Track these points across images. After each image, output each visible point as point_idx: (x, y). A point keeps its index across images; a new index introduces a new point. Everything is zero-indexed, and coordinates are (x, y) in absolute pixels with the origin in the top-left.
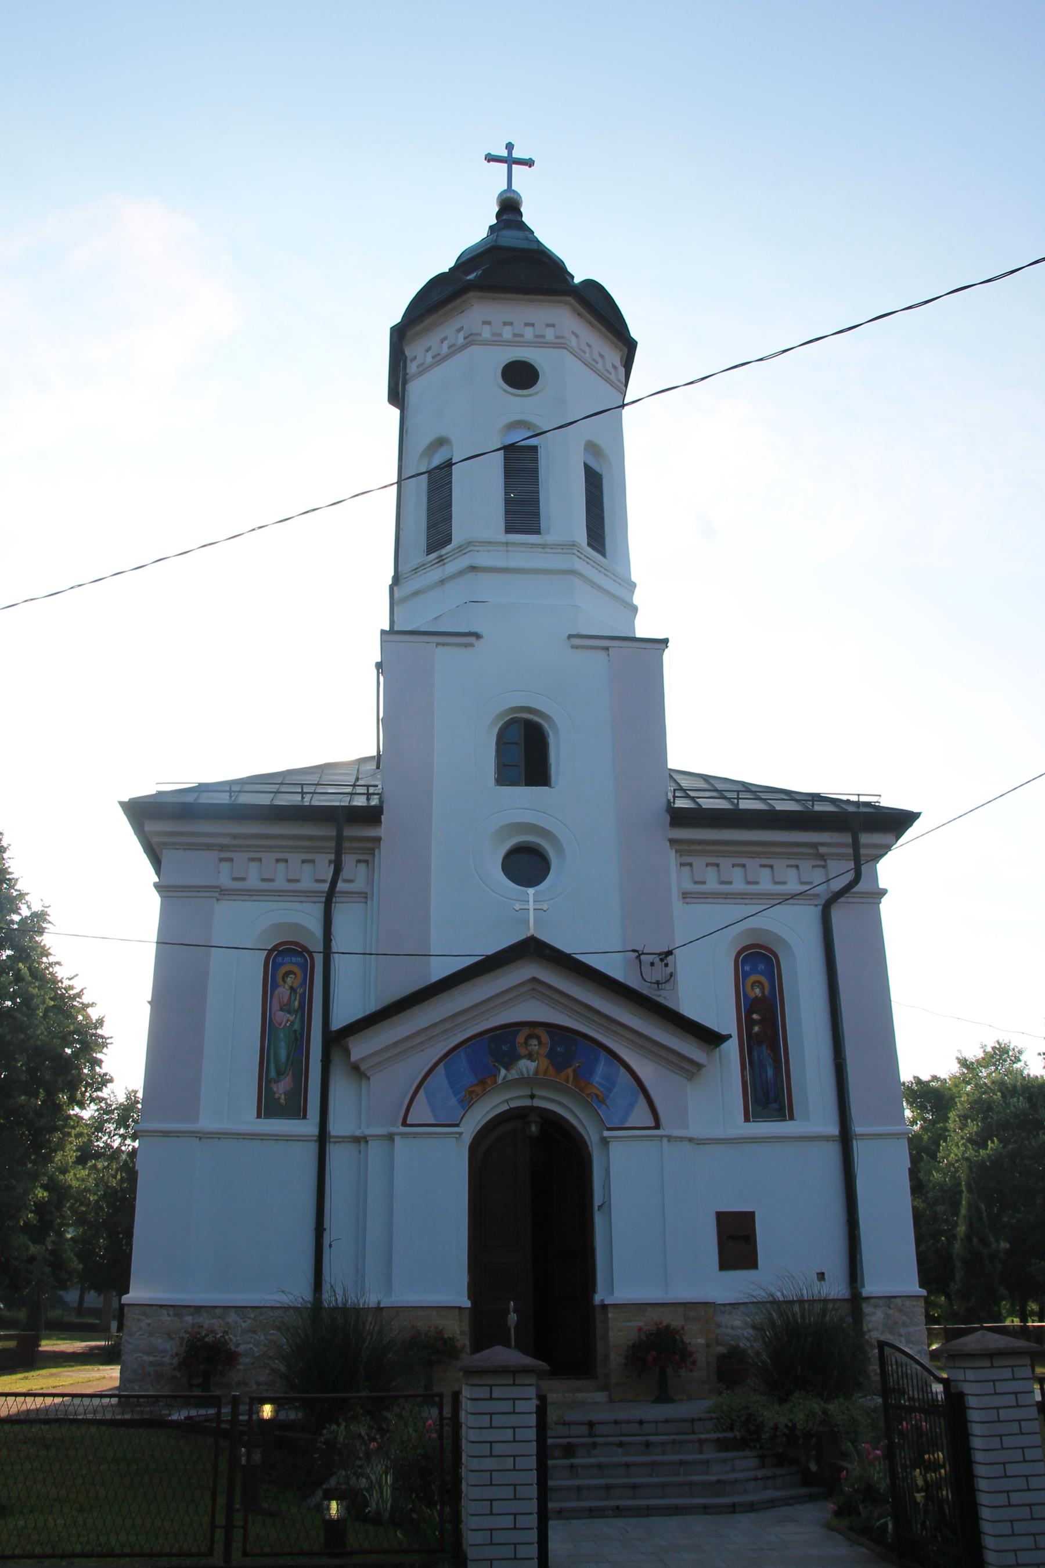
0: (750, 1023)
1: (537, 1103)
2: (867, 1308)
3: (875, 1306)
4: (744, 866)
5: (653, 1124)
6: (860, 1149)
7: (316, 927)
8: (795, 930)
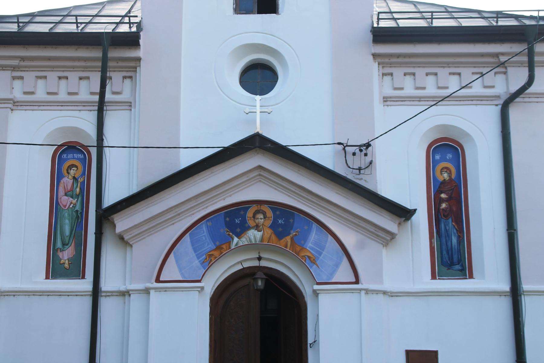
0: (438, 201)
1: (264, 263)
4: (436, 74)
5: (354, 280)
6: (527, 302)
7: (91, 130)
8: (478, 127)
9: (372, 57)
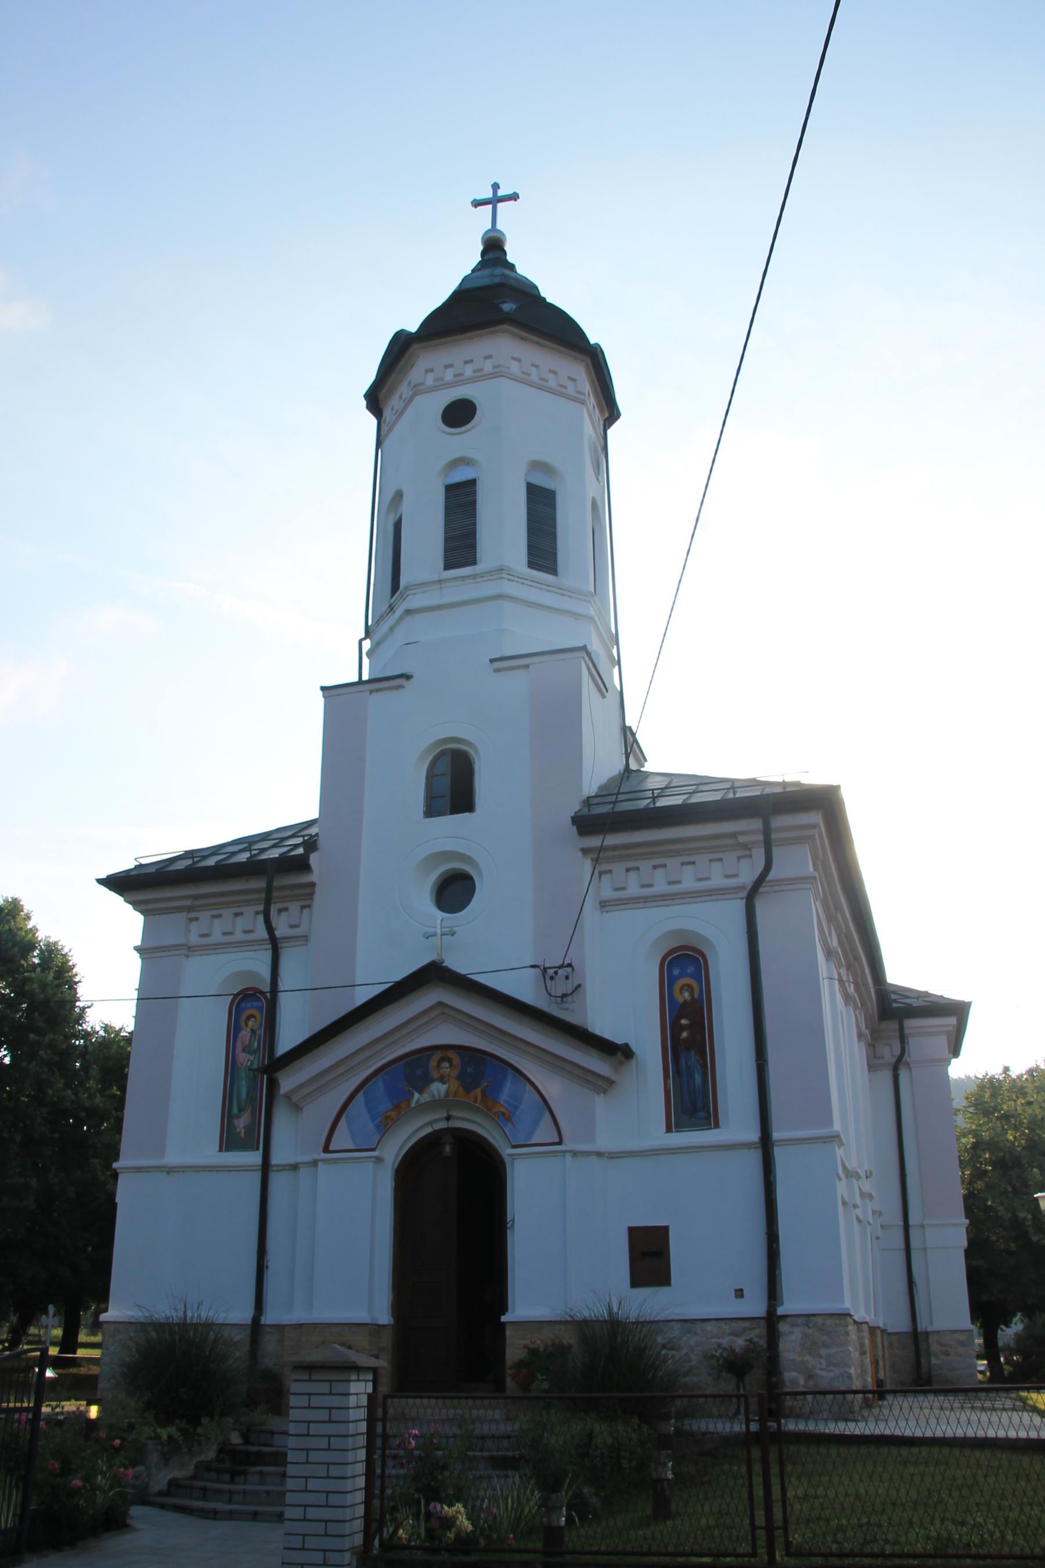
0: (677, 1029)
2: (783, 1327)
3: (793, 1325)
5: (557, 1140)
6: (778, 1152)
7: (266, 973)
8: (719, 928)
9: (580, 853)
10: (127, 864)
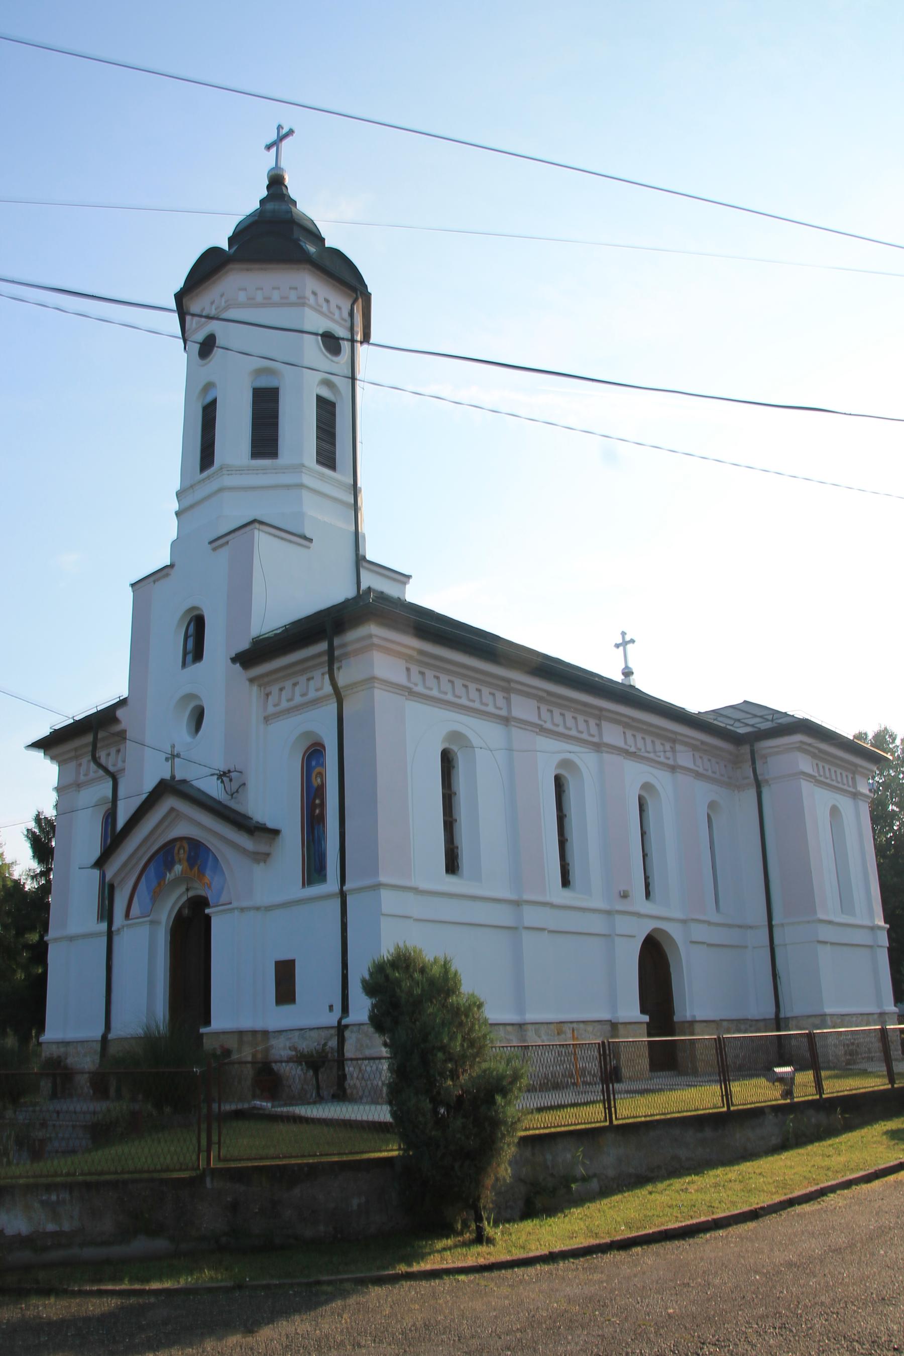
9: (247, 683)
10: (44, 731)
